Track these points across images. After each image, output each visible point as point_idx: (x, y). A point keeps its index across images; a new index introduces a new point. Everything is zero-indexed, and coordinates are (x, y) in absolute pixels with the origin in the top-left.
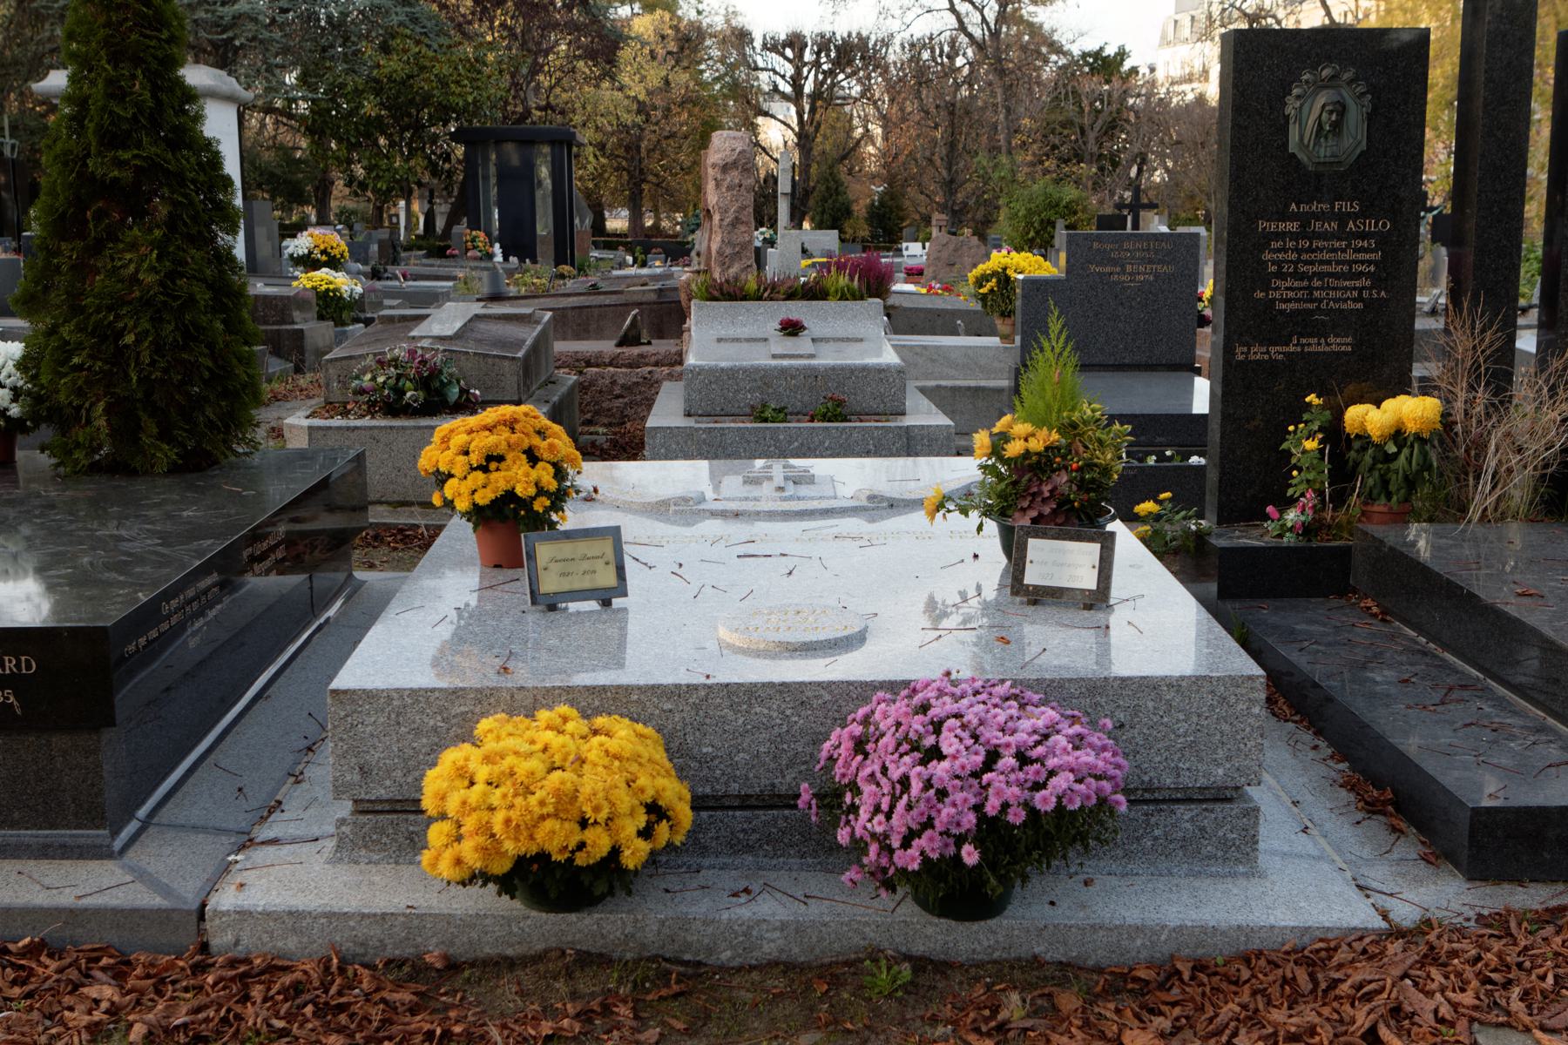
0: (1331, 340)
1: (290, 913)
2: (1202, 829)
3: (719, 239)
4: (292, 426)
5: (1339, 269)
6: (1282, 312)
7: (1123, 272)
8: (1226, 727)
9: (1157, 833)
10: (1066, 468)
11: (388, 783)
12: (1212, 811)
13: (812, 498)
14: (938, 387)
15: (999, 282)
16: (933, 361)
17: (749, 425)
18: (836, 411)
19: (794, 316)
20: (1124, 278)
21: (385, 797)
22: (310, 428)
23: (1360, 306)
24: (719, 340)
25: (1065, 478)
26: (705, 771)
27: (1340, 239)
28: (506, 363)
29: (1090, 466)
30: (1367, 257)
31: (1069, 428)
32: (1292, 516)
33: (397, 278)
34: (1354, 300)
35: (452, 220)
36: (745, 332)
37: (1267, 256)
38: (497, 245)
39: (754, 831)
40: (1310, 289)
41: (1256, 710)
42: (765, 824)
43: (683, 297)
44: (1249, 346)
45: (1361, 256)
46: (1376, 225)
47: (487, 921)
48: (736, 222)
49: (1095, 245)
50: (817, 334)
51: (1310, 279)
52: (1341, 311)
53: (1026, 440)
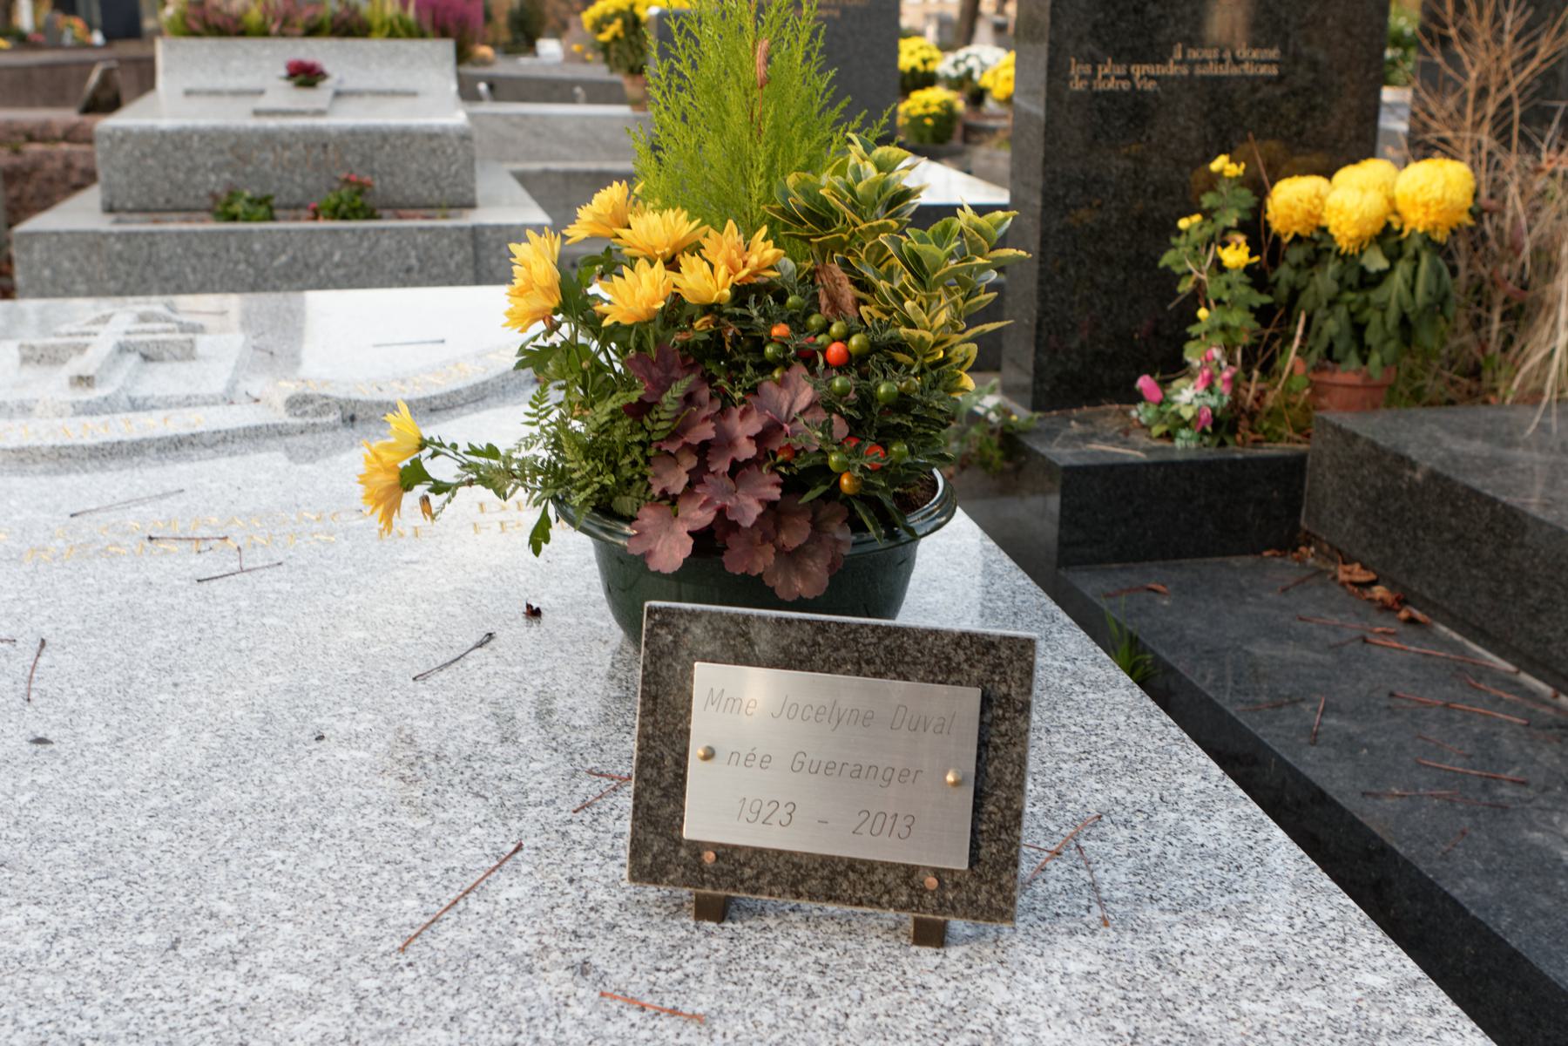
10: (808, 358)
13: (168, 404)
14: (546, 172)
15: (625, 25)
16: (537, 135)
17: (199, 227)
18: (356, 203)
24: (189, 93)
25: (806, 396)
29: (886, 352)
31: (809, 223)
32: (1187, 396)
36: (233, 83)
44: (1094, 62)
50: (350, 84)
53: (672, 264)
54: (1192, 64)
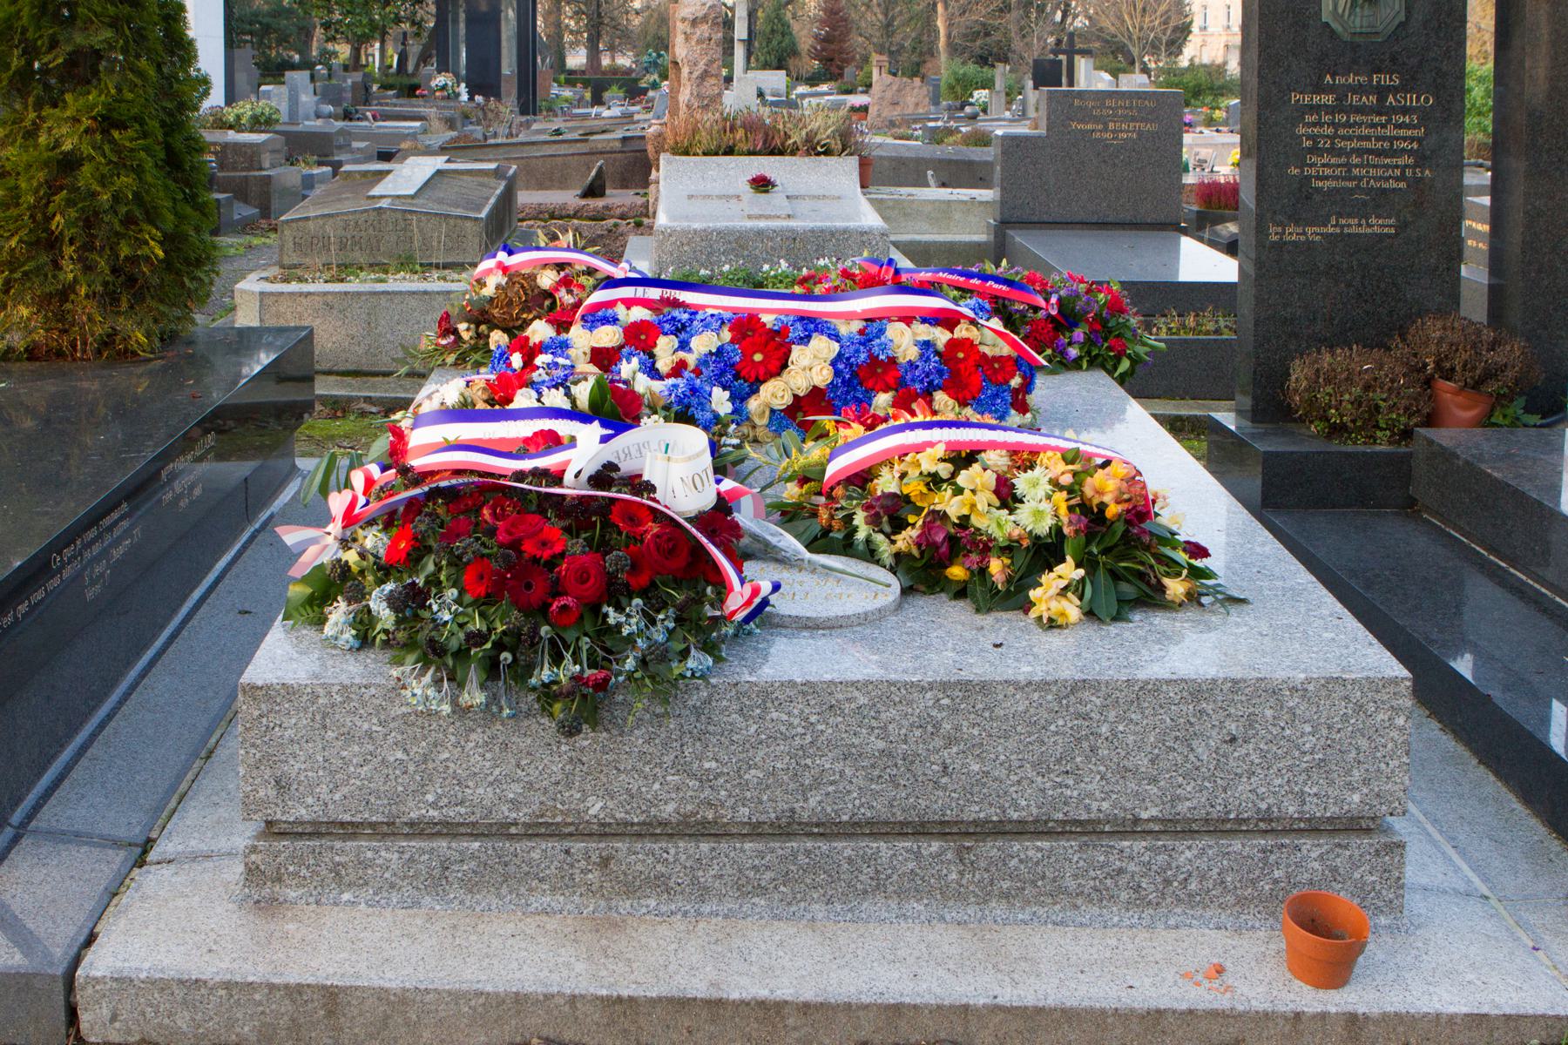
0: (1373, 221)
1: (181, 982)
2: (1334, 870)
3: (688, 92)
4: (243, 291)
5: (1379, 145)
6: (1318, 190)
7: (1106, 129)
8: (1363, 743)
9: (1277, 874)
11: (310, 800)
12: (1346, 847)
19: (771, 175)
20: (1107, 135)
21: (307, 818)
22: (262, 293)
23: (1402, 185)
24: (690, 197)
26: (707, 792)
27: (1380, 114)
28: (469, 224)
30: (1406, 133)
33: (366, 119)
34: (1397, 179)
35: (424, 59)
36: (716, 188)
37: (1301, 130)
38: (463, 85)
39: (768, 868)
40: (1349, 166)
41: (1400, 721)
42: (783, 859)
43: (650, 149)
45: (1402, 132)
46: (1418, 99)
47: (428, 998)
48: (705, 75)
49: (1076, 102)
51: (1348, 155)
52: (1384, 191)
54: (1342, 227)
